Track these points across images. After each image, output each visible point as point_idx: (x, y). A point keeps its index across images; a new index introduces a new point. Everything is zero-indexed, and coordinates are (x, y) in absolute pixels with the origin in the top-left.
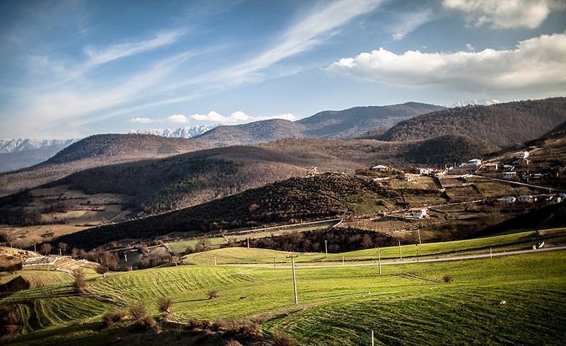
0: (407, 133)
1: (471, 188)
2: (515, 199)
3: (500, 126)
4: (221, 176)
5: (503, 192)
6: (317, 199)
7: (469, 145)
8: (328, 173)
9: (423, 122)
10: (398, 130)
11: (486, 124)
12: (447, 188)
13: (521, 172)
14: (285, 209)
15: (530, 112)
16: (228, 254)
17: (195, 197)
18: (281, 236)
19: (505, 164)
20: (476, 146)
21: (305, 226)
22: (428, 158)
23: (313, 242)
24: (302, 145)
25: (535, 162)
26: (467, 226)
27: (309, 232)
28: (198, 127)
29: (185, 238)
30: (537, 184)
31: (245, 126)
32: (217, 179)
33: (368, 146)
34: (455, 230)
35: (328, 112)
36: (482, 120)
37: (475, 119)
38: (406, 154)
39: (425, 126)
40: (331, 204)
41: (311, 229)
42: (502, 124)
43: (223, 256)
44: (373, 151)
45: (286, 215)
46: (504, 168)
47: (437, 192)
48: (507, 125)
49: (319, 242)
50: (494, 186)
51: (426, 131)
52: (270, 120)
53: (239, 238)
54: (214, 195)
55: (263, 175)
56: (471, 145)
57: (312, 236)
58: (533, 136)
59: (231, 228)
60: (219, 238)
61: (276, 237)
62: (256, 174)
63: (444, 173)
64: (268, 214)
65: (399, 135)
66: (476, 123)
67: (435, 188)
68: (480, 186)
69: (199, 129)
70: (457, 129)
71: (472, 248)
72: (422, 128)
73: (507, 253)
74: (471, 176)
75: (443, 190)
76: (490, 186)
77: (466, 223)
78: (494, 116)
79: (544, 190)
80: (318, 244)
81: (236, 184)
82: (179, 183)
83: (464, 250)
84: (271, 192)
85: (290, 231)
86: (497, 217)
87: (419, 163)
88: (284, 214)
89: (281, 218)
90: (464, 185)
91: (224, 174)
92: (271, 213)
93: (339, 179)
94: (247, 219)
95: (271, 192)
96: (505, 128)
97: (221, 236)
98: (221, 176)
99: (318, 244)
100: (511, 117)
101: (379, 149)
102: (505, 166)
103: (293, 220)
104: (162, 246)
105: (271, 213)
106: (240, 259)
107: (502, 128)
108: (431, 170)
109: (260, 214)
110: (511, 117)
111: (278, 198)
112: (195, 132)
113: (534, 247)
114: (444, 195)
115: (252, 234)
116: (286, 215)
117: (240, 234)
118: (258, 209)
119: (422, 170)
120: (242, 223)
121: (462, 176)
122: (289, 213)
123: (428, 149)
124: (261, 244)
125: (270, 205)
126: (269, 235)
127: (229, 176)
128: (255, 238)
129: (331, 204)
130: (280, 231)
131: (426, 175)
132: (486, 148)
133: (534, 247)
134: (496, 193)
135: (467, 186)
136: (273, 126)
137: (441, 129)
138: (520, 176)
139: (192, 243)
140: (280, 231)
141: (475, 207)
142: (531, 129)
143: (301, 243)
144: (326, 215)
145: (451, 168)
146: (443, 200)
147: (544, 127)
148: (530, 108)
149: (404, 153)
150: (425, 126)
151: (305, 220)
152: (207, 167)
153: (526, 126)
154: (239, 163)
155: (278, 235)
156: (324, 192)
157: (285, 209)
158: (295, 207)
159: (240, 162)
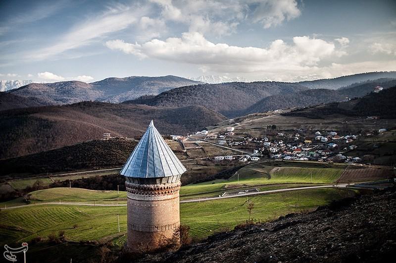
0: (167, 100)
1: (201, 150)
2: (223, 158)
3: (225, 99)
4: (40, 130)
5: (218, 153)
6: (110, 154)
7: (205, 113)
8: (117, 138)
9: (177, 93)
10: (161, 97)
11: (216, 97)
12: (187, 149)
13: (228, 140)
14: (90, 160)
15: (243, 90)
16: (59, 193)
17: (21, 144)
18: (88, 179)
19: (221, 135)
20: (209, 114)
21: (104, 172)
22: (179, 121)
23: (109, 183)
24: (97, 107)
25: (236, 134)
26: (197, 174)
27: (106, 176)
28: (13, 81)
29: (23, 178)
30: (236, 148)
31: (52, 84)
32: (38, 132)
33: (141, 110)
34: (190, 177)
35: (113, 78)
36: (215, 94)
37: (210, 93)
38: (166, 117)
39: (179, 96)
40: (119, 158)
41: (107, 174)
42: (226, 97)
43: (55, 194)
44: (144, 114)
45: (91, 165)
46: (219, 137)
47: (182, 152)
48: (230, 98)
49: (112, 183)
50: (213, 149)
51: (179, 99)
52: (71, 82)
53: (62, 179)
54: (35, 143)
55: (71, 130)
56: (206, 114)
57: (108, 179)
58: (244, 106)
59: (55, 171)
60: (47, 179)
61: (85, 179)
62: (65, 129)
63: (186, 139)
64: (79, 163)
65: (162, 102)
66: (210, 96)
67: (181, 149)
68: (206, 149)
69: (14, 83)
70: (199, 99)
71: (194, 193)
72: (177, 98)
73: (209, 199)
74: (202, 142)
75: (185, 151)
76: (211, 149)
77: (196, 172)
78: (222, 92)
79: (239, 152)
80: (111, 184)
81: (51, 136)
82: (9, 133)
83: (191, 195)
84: (81, 149)
85: (94, 175)
86: (213, 169)
87: (174, 123)
88: (89, 164)
89: (87, 166)
90: (197, 148)
91: (42, 128)
92: (81, 163)
93: (124, 142)
94: (65, 166)
95: (81, 149)
96: (228, 100)
97: (48, 178)
98: (40, 130)
99: (111, 184)
100: (232, 94)
101: (148, 112)
102: (221, 136)
103: (95, 168)
104: (6, 184)
105: (81, 163)
106: (67, 196)
107: (226, 100)
108: (179, 137)
109: (73, 163)
110: (232, 94)
111: (85, 153)
112: (11, 84)
113: (220, 196)
114: (186, 154)
115: (69, 177)
116: (91, 165)
117: (60, 176)
118: (72, 160)
119: (173, 138)
120: (62, 169)
121: (196, 142)
122: (93, 163)
123: (180, 114)
124: (76, 184)
125: (80, 157)
126: (80, 177)
127: (46, 130)
128: (72, 179)
129: (119, 158)
130: (87, 175)
131: (176, 140)
132: (215, 115)
133: (220, 196)
134: (214, 153)
135: (198, 149)
136: (73, 86)
137: (189, 99)
138: (228, 143)
139: (31, 182)
140: (87, 175)
141: (202, 162)
142: (243, 101)
143: (101, 183)
144: (116, 165)
145: (191, 136)
146: (185, 157)
147: (251, 101)
148: (244, 88)
149: (164, 116)
150: (179, 96)
151: (103, 168)
152: (30, 122)
153: (240, 99)
154: (53, 121)
155: (87, 178)
156: (115, 150)
157: (90, 160)
158: (96, 159)
159: (54, 120)
